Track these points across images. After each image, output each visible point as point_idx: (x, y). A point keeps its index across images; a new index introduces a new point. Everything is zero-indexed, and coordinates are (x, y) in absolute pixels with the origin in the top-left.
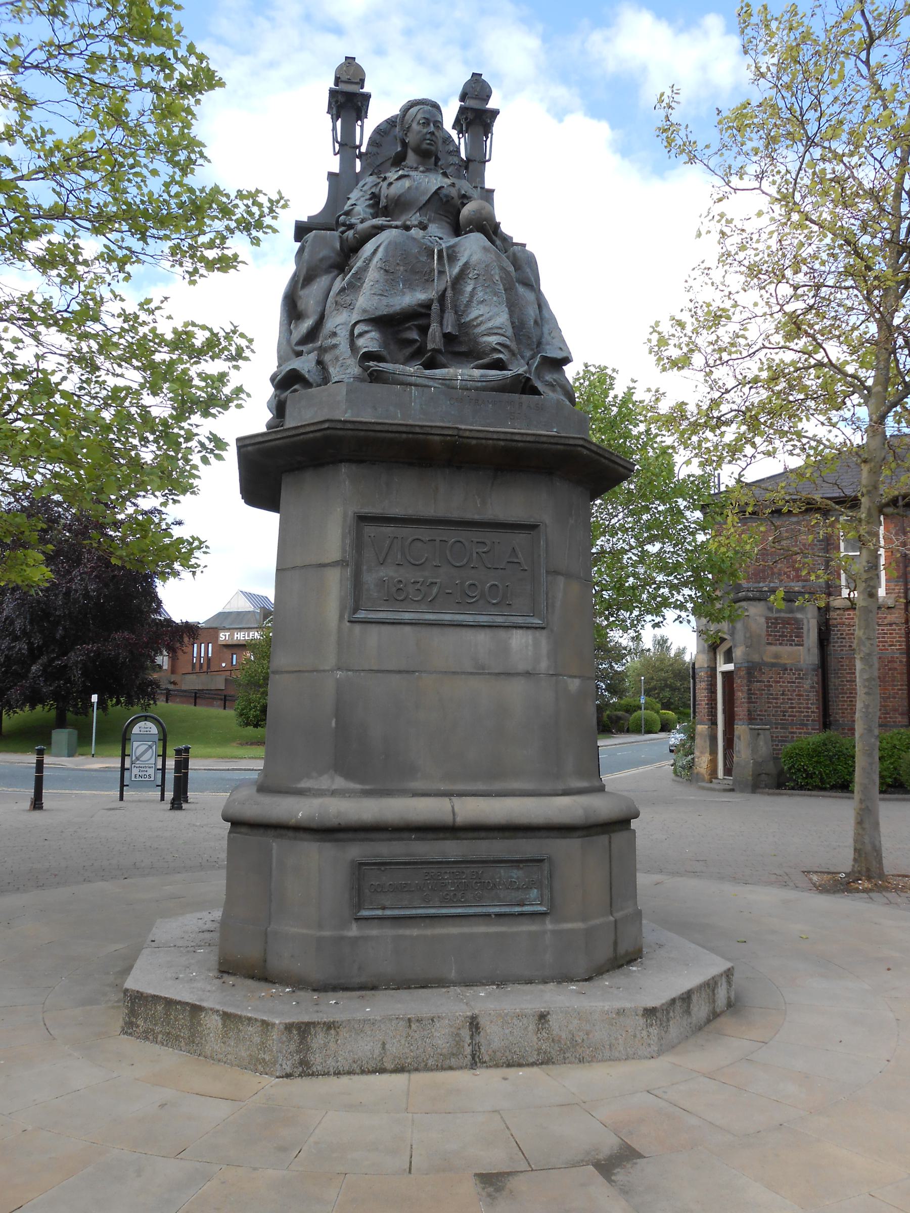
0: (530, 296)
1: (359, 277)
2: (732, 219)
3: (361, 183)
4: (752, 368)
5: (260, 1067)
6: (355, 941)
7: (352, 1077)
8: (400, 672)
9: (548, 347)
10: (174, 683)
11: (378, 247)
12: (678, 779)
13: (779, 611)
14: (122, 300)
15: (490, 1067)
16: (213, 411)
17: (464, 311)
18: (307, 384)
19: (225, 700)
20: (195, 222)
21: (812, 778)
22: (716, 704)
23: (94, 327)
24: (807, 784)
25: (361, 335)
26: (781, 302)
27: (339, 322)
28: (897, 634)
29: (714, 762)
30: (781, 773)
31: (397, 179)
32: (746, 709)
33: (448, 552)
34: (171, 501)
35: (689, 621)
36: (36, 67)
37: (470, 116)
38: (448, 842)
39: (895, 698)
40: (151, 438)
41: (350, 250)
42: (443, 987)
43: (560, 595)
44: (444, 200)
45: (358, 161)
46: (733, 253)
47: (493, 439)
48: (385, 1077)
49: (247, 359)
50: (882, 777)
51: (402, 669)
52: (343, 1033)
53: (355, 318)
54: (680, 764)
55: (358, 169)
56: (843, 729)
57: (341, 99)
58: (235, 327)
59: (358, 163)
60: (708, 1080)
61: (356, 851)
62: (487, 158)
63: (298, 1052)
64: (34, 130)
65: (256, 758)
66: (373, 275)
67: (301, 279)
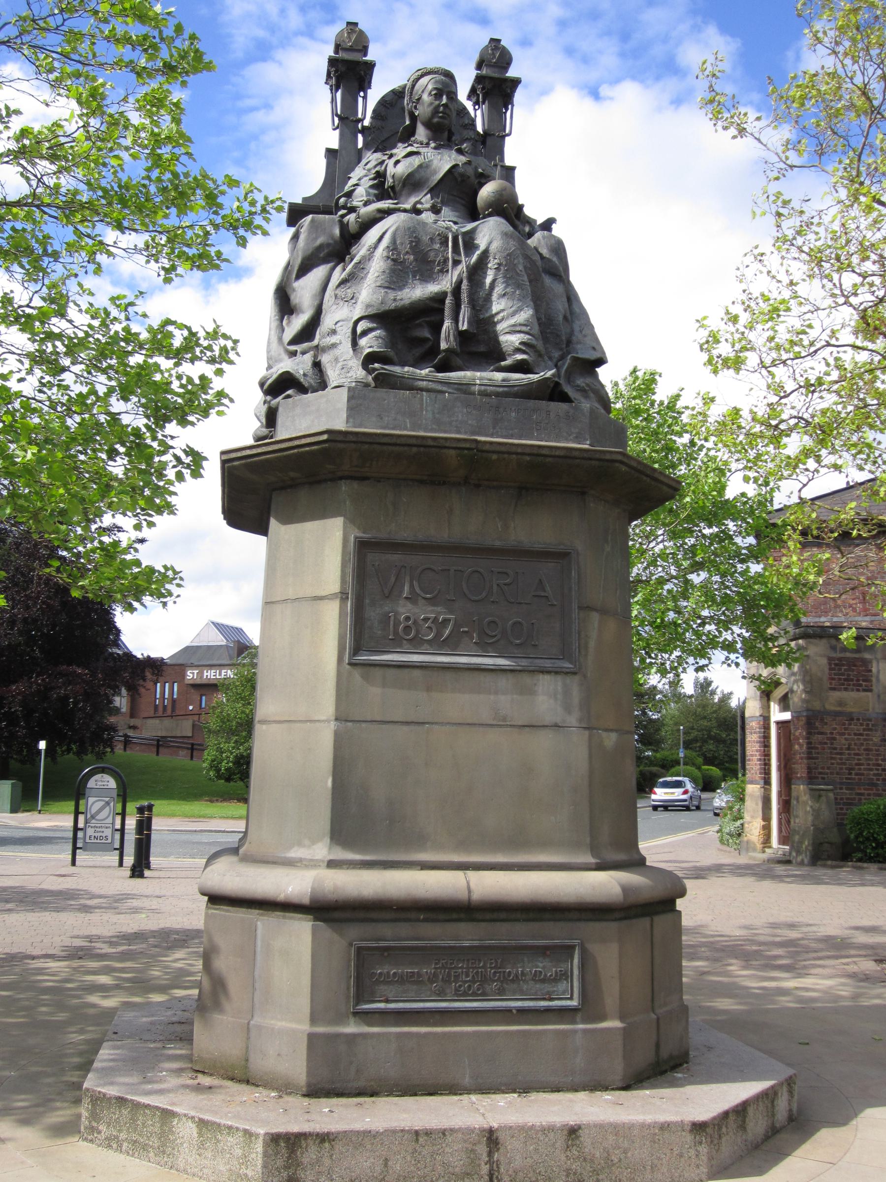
0: (558, 288)
1: (361, 267)
2: (790, 201)
3: (364, 161)
4: (814, 368)
6: (353, 1037)
8: (407, 723)
10: (134, 728)
11: (384, 233)
14: (91, 294)
16: (191, 418)
17: (483, 306)
19: (192, 749)
20: (182, 208)
22: (769, 760)
23: (57, 325)
24: (878, 855)
25: (365, 333)
27: (340, 316)
29: (767, 828)
30: (846, 842)
33: (464, 586)
34: (144, 524)
35: (737, 665)
37: (488, 86)
40: (122, 450)
41: (350, 238)
42: (456, 1094)
43: (594, 634)
46: (791, 237)
47: (517, 454)
49: (231, 362)
52: (339, 1146)
53: (358, 312)
54: (727, 830)
55: (360, 144)
57: (342, 68)
58: (218, 327)
59: (360, 138)
61: (355, 931)
62: (507, 131)
63: (286, 1168)
65: (227, 818)
66: (377, 266)
67: (296, 269)
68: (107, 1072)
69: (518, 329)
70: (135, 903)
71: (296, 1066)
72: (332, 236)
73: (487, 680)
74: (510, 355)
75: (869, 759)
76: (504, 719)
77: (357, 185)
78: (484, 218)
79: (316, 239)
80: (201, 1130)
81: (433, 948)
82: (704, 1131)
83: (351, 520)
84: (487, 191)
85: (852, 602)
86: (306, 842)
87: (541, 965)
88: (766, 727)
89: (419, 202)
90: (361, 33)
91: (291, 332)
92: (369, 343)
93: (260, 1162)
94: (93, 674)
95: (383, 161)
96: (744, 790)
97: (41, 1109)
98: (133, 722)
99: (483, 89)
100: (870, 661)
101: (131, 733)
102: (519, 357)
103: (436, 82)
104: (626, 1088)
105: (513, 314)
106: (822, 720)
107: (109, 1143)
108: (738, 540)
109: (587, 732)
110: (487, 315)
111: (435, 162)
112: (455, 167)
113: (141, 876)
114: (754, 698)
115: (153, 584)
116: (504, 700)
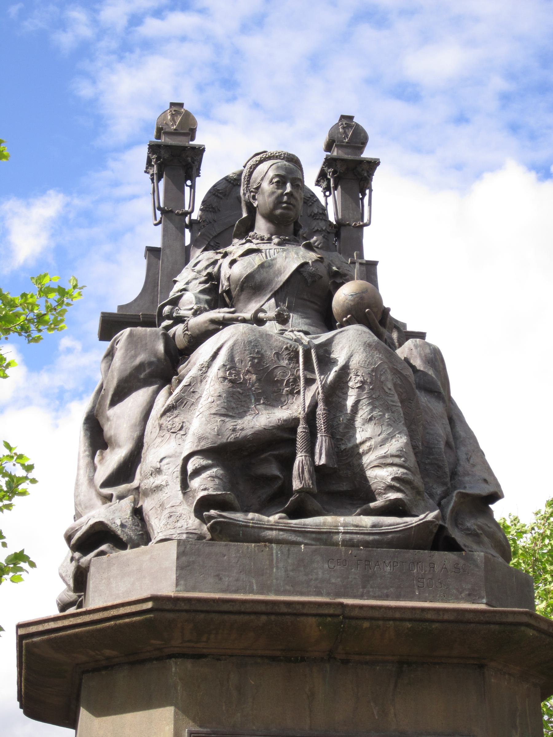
0: (437, 407)
1: (191, 390)
3: (192, 262)
9: (467, 479)
17: (344, 434)
18: (120, 544)
25: (197, 472)
27: (165, 452)
37: (341, 168)
41: (177, 355)
44: (310, 280)
45: (187, 231)
47: (395, 619)
53: (188, 447)
55: (188, 242)
66: (211, 389)
67: (111, 393)
69: (390, 461)
72: (155, 354)
74: (380, 494)
77: (185, 290)
78: (341, 326)
79: (135, 356)
83: (184, 710)
84: (344, 294)
90: (187, 115)
91: (105, 470)
92: (203, 485)
99: (334, 172)
102: (393, 496)
103: (278, 168)
105: (382, 443)
110: (350, 445)
112: (304, 265)
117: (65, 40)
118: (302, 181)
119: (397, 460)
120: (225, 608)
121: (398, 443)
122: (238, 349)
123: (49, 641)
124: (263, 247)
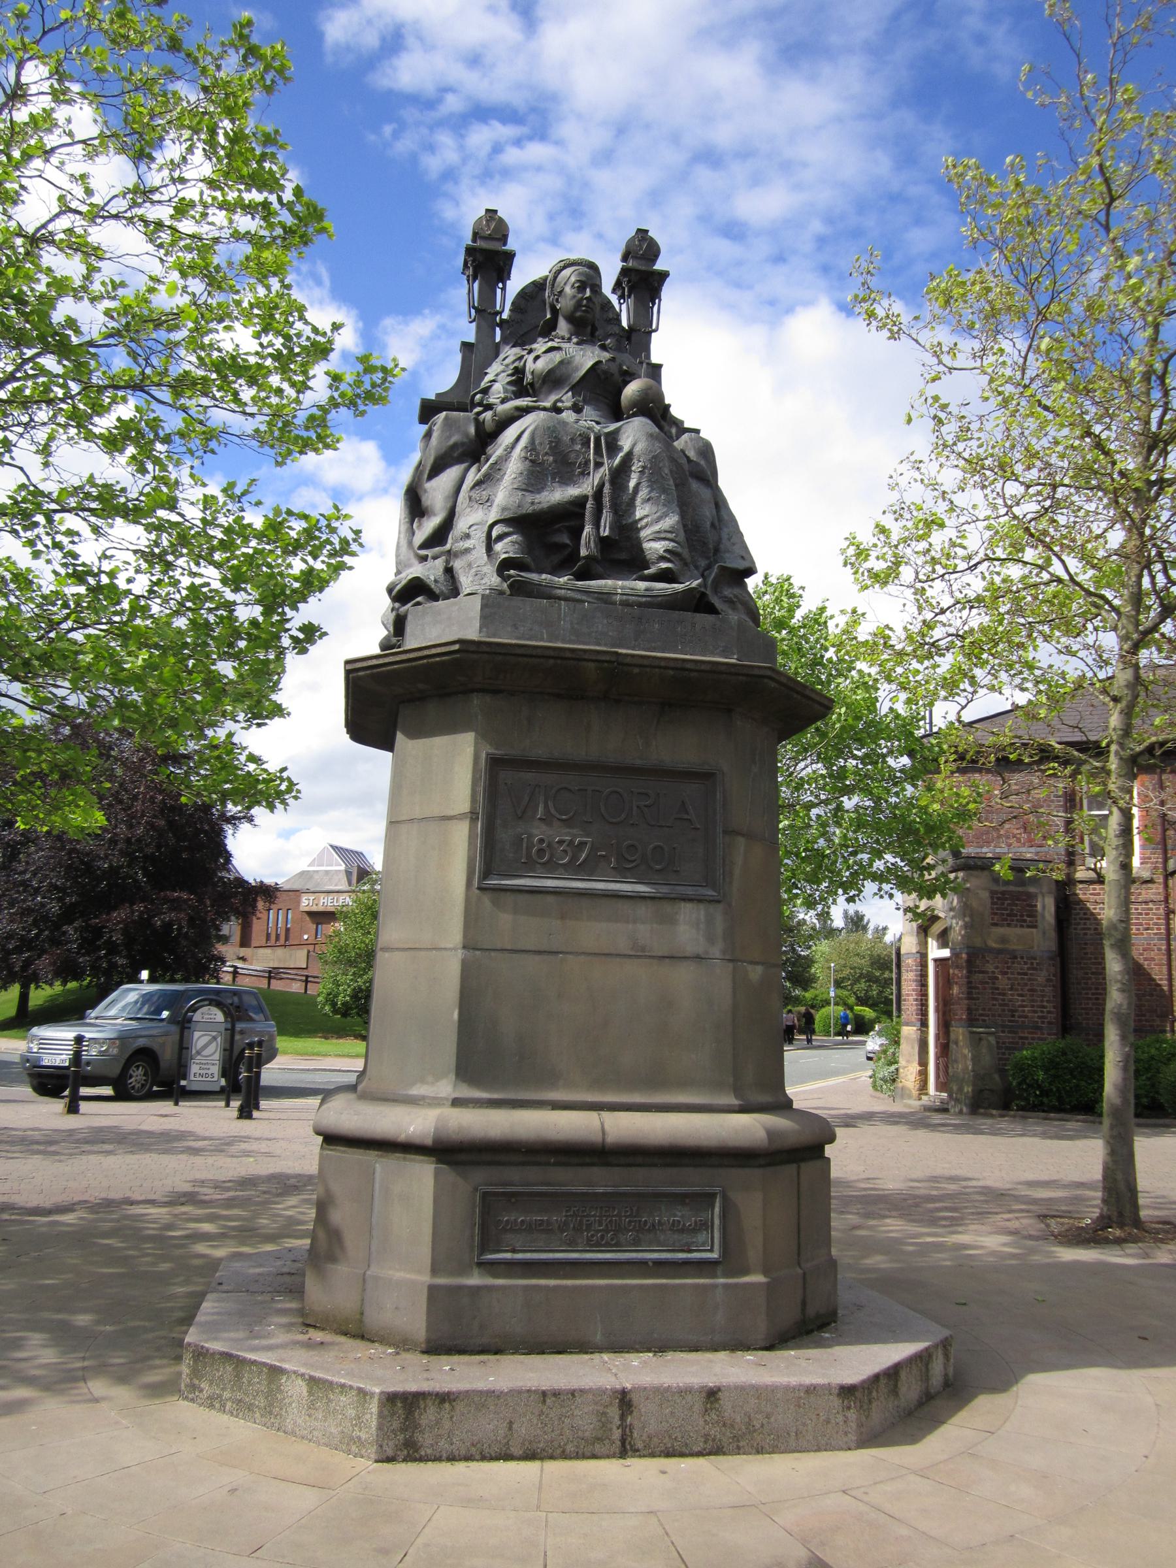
0: (705, 493)
1: (498, 468)
3: (502, 356)
5: (354, 1448)
6: (478, 1289)
7: (471, 1464)
8: (539, 952)
9: (727, 555)
10: (243, 959)
12: (878, 1094)
13: (1008, 883)
15: (644, 1456)
17: (626, 511)
18: (433, 596)
19: (307, 982)
21: (1047, 1096)
22: (927, 1000)
25: (500, 538)
26: (1009, 502)
27: (473, 520)
28: (1155, 914)
29: (923, 1074)
31: (545, 352)
32: (965, 1007)
36: (116, 217)
37: (634, 278)
38: (595, 1169)
39: (1152, 995)
41: (486, 437)
42: (586, 1353)
44: (603, 377)
45: (498, 329)
46: (951, 442)
47: (660, 667)
48: (512, 1465)
50: (1137, 1097)
51: (542, 949)
52: (460, 1407)
53: (493, 516)
54: (881, 1076)
55: (498, 339)
56: (1088, 1034)
60: (919, 1479)
61: (481, 1176)
64: (103, 283)
65: (344, 1056)
66: (514, 468)
67: (428, 468)
68: (213, 1328)
69: (663, 535)
70: (243, 1146)
71: (414, 1320)
72: (467, 435)
73: (625, 907)
74: (653, 563)
75: (1033, 1001)
76: (643, 950)
77: (494, 381)
78: (628, 418)
79: (449, 437)
80: (311, 1388)
81: (564, 1194)
82: (853, 1395)
83: (483, 735)
84: (631, 390)
85: (1016, 832)
86: (430, 1079)
87: (679, 1214)
88: (923, 965)
89: (560, 400)
90: (501, 220)
91: (421, 536)
92: (503, 549)
93: (374, 1424)
94: (200, 900)
95: (523, 356)
96: (899, 1032)
97: (138, 1366)
98: (243, 952)
99: (629, 282)
100: (1035, 896)
101: (239, 964)
102: (664, 565)
103: (580, 274)
104: (770, 1348)
105: (658, 520)
106: (984, 957)
107: (212, 1402)
108: (890, 761)
109: (731, 965)
110: (630, 521)
111: (577, 358)
112: (598, 363)
113: (250, 1117)
114: (910, 933)
115: (269, 791)
116: (643, 929)
117: (433, 164)
118: (600, 287)
119: (669, 536)
120: (519, 651)
121: (671, 521)
122: (538, 433)
123: (372, 675)
124: (563, 345)
